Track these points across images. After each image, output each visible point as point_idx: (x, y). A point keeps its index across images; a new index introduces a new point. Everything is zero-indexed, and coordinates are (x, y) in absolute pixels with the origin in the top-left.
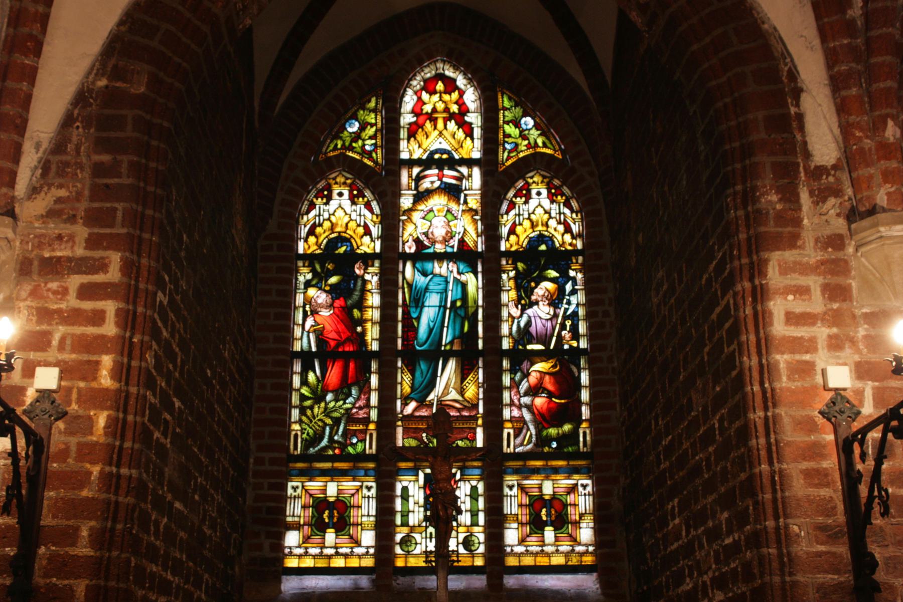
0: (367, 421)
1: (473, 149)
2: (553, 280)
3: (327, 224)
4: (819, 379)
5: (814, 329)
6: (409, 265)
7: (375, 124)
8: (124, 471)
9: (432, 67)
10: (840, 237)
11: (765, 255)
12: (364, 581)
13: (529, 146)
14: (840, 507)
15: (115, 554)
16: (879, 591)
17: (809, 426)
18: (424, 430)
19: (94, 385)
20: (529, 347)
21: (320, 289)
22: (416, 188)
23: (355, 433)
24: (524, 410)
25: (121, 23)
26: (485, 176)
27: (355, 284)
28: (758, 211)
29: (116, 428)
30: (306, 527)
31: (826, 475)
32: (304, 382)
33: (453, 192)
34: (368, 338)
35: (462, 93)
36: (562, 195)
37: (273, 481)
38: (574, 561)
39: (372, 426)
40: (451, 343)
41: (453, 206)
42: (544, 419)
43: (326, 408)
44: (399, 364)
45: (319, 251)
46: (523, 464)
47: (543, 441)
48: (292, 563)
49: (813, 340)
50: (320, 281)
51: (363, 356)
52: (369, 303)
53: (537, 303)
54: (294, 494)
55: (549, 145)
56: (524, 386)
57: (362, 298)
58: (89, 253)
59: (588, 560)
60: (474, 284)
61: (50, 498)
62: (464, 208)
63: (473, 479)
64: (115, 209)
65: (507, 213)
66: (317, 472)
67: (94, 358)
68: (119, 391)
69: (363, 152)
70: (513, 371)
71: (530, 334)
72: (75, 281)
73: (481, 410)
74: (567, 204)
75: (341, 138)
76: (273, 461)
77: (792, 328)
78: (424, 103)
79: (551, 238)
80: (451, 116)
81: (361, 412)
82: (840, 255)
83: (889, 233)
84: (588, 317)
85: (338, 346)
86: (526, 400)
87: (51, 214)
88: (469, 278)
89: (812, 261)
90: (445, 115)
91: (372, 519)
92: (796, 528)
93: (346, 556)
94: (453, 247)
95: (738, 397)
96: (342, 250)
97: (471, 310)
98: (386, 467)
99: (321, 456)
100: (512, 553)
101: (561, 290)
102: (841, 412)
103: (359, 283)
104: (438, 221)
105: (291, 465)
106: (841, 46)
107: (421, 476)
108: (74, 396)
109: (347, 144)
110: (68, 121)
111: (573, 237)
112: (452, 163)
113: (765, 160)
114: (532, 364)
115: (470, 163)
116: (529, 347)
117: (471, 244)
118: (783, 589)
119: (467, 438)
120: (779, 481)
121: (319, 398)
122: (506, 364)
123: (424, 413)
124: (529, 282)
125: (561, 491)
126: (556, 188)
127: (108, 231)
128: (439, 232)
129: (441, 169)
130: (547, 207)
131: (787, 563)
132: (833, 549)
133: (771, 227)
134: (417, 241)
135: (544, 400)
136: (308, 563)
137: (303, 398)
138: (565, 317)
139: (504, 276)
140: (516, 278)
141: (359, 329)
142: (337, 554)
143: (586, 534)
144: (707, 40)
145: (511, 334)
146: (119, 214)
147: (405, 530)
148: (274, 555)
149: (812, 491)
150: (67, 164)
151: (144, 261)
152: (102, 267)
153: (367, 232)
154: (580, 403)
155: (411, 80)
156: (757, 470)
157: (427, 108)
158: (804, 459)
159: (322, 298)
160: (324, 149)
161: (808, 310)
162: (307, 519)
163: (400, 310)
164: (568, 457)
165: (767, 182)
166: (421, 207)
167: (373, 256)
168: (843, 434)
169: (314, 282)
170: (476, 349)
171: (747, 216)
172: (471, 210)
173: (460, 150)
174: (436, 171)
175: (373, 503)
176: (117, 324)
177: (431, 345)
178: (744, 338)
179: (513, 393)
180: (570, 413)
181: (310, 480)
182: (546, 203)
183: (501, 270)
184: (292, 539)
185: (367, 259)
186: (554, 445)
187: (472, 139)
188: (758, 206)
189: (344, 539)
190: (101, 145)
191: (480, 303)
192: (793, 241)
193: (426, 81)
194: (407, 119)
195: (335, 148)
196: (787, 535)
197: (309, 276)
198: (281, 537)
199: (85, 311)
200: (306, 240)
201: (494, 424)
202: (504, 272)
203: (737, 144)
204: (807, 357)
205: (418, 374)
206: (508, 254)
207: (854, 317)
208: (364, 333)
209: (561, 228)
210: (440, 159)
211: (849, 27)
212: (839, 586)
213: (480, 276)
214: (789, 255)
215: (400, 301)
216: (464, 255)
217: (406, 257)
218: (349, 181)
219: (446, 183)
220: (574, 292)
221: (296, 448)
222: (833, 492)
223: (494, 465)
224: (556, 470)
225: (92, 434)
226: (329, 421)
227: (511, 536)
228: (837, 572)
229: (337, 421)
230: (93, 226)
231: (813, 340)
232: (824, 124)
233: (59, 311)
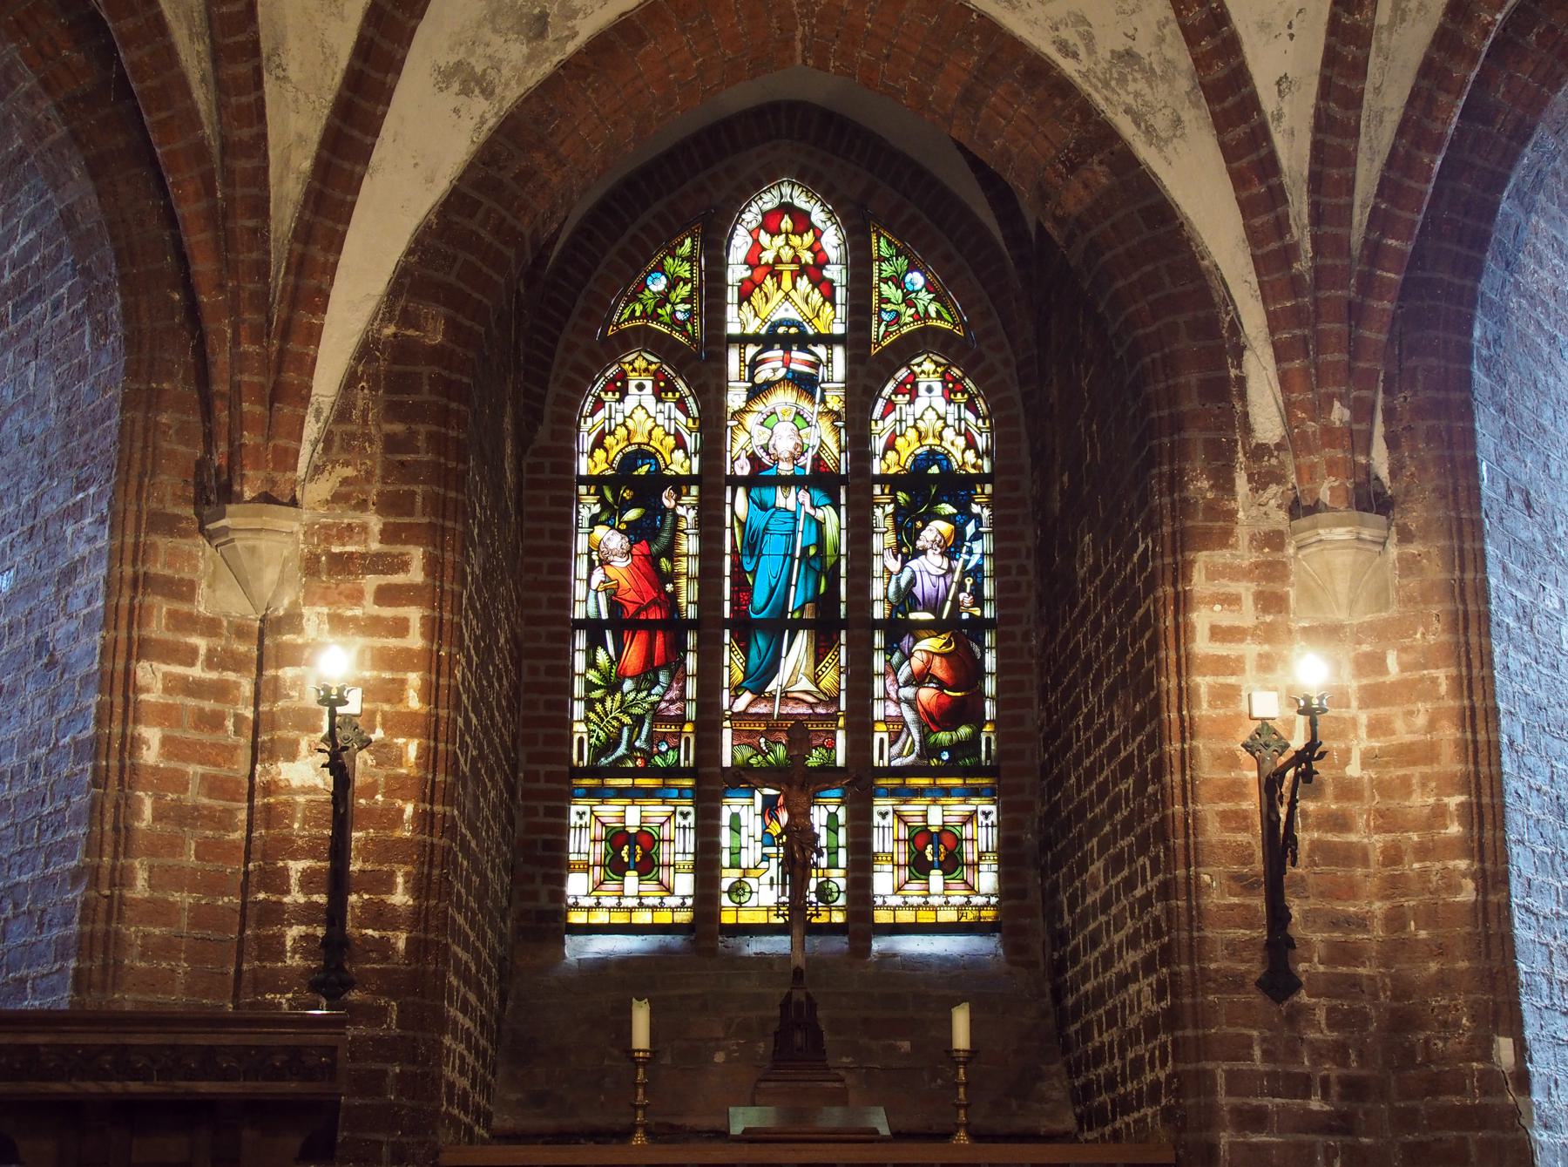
0: (681, 720)
1: (834, 321)
2: (948, 518)
3: (621, 432)
4: (1244, 706)
5: (1243, 646)
6: (741, 492)
7: (691, 280)
8: (438, 808)
9: (775, 192)
10: (1280, 534)
11: (1190, 555)
13: (916, 317)
14: (1259, 854)
15: (433, 902)
16: (1294, 947)
17: (1232, 761)
18: (762, 734)
19: (401, 708)
20: (913, 616)
21: (612, 527)
22: (751, 379)
23: (664, 737)
24: (904, 706)
25: (410, 252)
26: (851, 361)
27: (663, 521)
28: (1185, 500)
29: (429, 758)
30: (597, 869)
31: (1245, 818)
32: (592, 664)
33: (805, 384)
34: (683, 600)
35: (818, 235)
36: (964, 391)
37: (552, 804)
38: (970, 916)
39: (688, 728)
40: (802, 608)
41: (805, 404)
42: (932, 720)
43: (622, 702)
44: (727, 639)
45: (610, 472)
46: (901, 783)
47: (929, 750)
48: (576, 918)
49: (1240, 660)
50: (613, 515)
51: (674, 626)
52: (683, 549)
53: (924, 552)
54: (579, 822)
55: (946, 316)
56: (904, 672)
57: (673, 543)
58: (385, 548)
59: (988, 914)
60: (834, 522)
61: (358, 840)
62: (821, 408)
63: (831, 804)
64: (414, 493)
65: (883, 417)
66: (612, 793)
67: (400, 675)
68: (429, 714)
69: (673, 322)
70: (889, 650)
71: (914, 596)
72: (371, 582)
73: (843, 706)
74: (970, 405)
75: (640, 301)
76: (550, 777)
77: (1218, 644)
78: (764, 249)
79: (946, 456)
80: (802, 270)
81: (672, 707)
82: (1278, 556)
83: (1330, 537)
84: (997, 573)
85: (638, 612)
86: (908, 692)
87: (337, 498)
88: (828, 515)
89: (1245, 564)
90: (794, 267)
91: (690, 857)
92: (1207, 878)
93: (653, 908)
94: (804, 467)
95: (1154, 723)
96: (643, 470)
97: (830, 561)
98: (709, 787)
99: (617, 770)
100: (884, 906)
101: (959, 534)
102: (1267, 746)
103: (669, 520)
104: (780, 427)
105: (575, 781)
106: (1283, 309)
107: (758, 797)
108: (379, 718)
109: (649, 310)
110: (350, 381)
111: (978, 456)
112: (803, 340)
113: (1195, 436)
114: (916, 641)
115: (829, 340)
116: (913, 616)
117: (831, 464)
118: (1191, 946)
119: (822, 746)
120: (1192, 824)
121: (613, 687)
122: (879, 640)
123: (762, 708)
124: (914, 521)
125: (953, 820)
126: (956, 381)
127: (406, 520)
128: (784, 443)
129: (787, 350)
130: (942, 412)
131: (1196, 917)
132: (1248, 901)
133: (1198, 521)
134: (753, 459)
135: (933, 691)
136: (600, 917)
137: (590, 687)
138: (965, 574)
139: (878, 512)
140: (894, 515)
141: (669, 587)
142: (641, 905)
143: (987, 880)
144: (1135, 277)
145: (886, 597)
146: (419, 499)
147: (737, 873)
148: (552, 906)
149: (1229, 837)
150: (353, 436)
151: (449, 556)
152: (404, 566)
153: (680, 444)
154: (982, 696)
155: (743, 212)
156: (1169, 812)
157: (768, 257)
158: (1222, 799)
159: (614, 541)
160: (616, 318)
161: (1237, 623)
162: (598, 858)
163: (728, 560)
164: (965, 773)
165: (1198, 464)
166: (758, 406)
167: (689, 480)
168: (1269, 768)
169: (603, 518)
170: (838, 620)
171: (1173, 504)
172: (831, 411)
173: (815, 321)
174: (781, 353)
175: (691, 836)
176: (423, 635)
177: (772, 610)
178: (1163, 654)
179: (888, 682)
180: (963, 711)
181: (602, 803)
182: (940, 404)
183: (871, 503)
184: (577, 885)
185: (679, 484)
186: (945, 756)
187: (834, 305)
188: (1185, 494)
189: (650, 887)
190: (394, 411)
191: (843, 550)
192: (1223, 539)
193: (765, 214)
194: (736, 272)
195: (632, 316)
196: (1197, 886)
197: (596, 509)
198: (561, 881)
199: (385, 619)
200: (591, 456)
202: (878, 505)
203: (1165, 413)
204: (1232, 680)
205: (753, 653)
206: (883, 479)
207: (1290, 631)
208: (675, 594)
209: (961, 441)
210: (787, 334)
211: (1295, 285)
212: (1251, 942)
213: (843, 510)
214: (1221, 557)
215: (728, 549)
216: (820, 479)
217: (735, 481)
218: (653, 367)
219: (794, 372)
220: (977, 536)
221: (581, 757)
222: (1252, 839)
223: (861, 784)
224: (948, 792)
225: (401, 766)
226: (627, 720)
227: (883, 882)
228: (1250, 926)
229: (638, 721)
230: (388, 515)
231: (1240, 660)
232: (1269, 392)
233: (354, 619)
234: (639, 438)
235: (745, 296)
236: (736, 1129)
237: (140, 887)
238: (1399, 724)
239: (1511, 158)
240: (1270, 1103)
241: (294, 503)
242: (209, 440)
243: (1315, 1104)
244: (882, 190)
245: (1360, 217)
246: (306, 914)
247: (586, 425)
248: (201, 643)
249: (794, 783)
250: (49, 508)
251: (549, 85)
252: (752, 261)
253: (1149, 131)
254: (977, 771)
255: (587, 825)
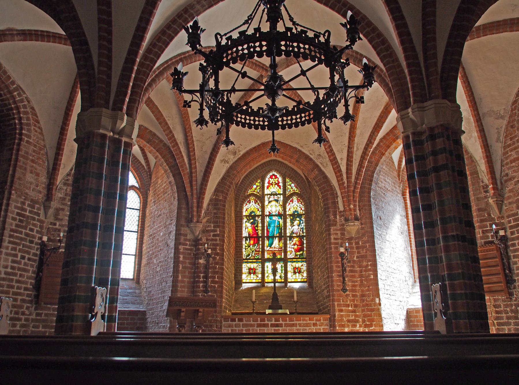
0: (259, 251)
12: (259, 284)
26: (283, 197)
33: (277, 201)
38: (303, 280)
41: (277, 204)
42: (297, 251)
46: (292, 260)
47: (296, 255)
56: (292, 244)
59: (305, 280)
60: (281, 221)
69: (257, 192)
70: (290, 240)
72: (212, 234)
74: (301, 203)
80: (276, 184)
86: (293, 247)
87: (207, 221)
98: (263, 261)
99: (249, 259)
101: (300, 223)
104: (273, 208)
110: (209, 205)
112: (276, 194)
122: (288, 239)
123: (271, 249)
134: (269, 212)
137: (246, 246)
143: (305, 274)
153: (258, 210)
157: (271, 182)
159: (249, 225)
164: (301, 258)
170: (282, 236)
182: (297, 203)
184: (244, 276)
185: (258, 216)
190: (215, 209)
194: (266, 185)
198: (241, 275)
201: (286, 252)
211: (344, 188)
216: (279, 215)
217: (267, 216)
223: (285, 261)
224: (299, 262)
227: (289, 275)
229: (253, 251)
234: (253, 209)
235: (268, 188)
236: (267, 313)
237: (180, 278)
238: (361, 252)
239: (375, 169)
240: (344, 308)
241: (201, 223)
242: (188, 213)
243: (350, 308)
244: (288, 173)
245: (353, 178)
246: (202, 282)
247: (244, 208)
248: (188, 243)
249: (274, 260)
250: (167, 223)
251: (236, 161)
252: (269, 183)
253: (323, 166)
254: (303, 258)
255: (245, 267)
